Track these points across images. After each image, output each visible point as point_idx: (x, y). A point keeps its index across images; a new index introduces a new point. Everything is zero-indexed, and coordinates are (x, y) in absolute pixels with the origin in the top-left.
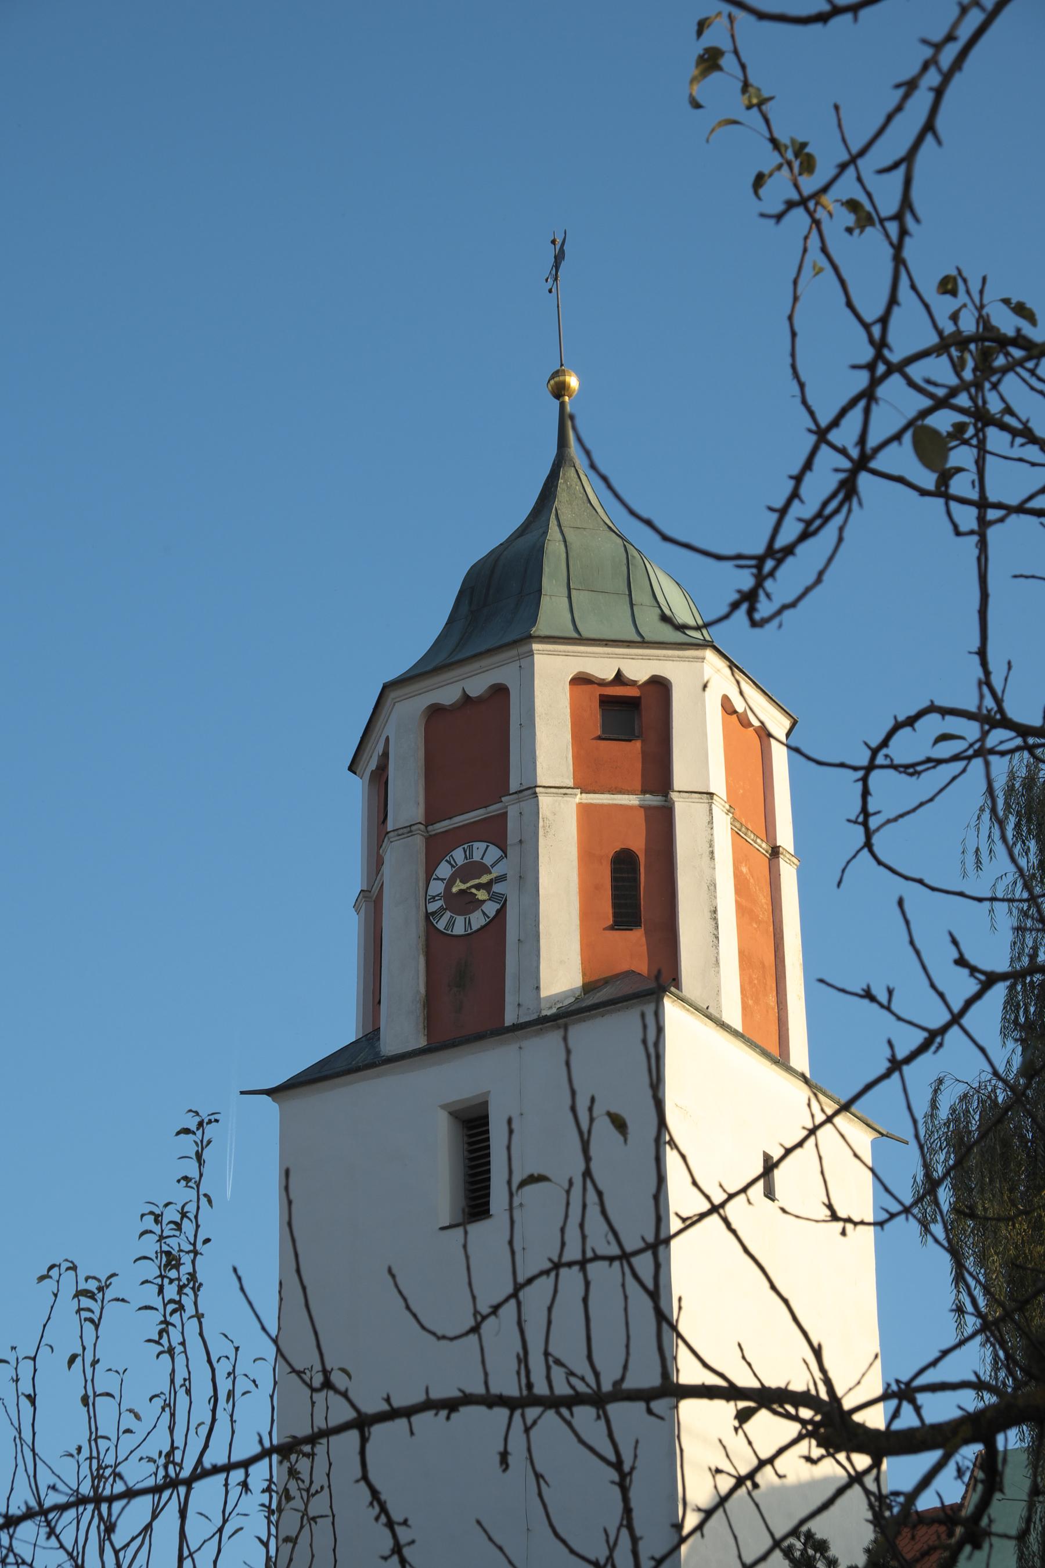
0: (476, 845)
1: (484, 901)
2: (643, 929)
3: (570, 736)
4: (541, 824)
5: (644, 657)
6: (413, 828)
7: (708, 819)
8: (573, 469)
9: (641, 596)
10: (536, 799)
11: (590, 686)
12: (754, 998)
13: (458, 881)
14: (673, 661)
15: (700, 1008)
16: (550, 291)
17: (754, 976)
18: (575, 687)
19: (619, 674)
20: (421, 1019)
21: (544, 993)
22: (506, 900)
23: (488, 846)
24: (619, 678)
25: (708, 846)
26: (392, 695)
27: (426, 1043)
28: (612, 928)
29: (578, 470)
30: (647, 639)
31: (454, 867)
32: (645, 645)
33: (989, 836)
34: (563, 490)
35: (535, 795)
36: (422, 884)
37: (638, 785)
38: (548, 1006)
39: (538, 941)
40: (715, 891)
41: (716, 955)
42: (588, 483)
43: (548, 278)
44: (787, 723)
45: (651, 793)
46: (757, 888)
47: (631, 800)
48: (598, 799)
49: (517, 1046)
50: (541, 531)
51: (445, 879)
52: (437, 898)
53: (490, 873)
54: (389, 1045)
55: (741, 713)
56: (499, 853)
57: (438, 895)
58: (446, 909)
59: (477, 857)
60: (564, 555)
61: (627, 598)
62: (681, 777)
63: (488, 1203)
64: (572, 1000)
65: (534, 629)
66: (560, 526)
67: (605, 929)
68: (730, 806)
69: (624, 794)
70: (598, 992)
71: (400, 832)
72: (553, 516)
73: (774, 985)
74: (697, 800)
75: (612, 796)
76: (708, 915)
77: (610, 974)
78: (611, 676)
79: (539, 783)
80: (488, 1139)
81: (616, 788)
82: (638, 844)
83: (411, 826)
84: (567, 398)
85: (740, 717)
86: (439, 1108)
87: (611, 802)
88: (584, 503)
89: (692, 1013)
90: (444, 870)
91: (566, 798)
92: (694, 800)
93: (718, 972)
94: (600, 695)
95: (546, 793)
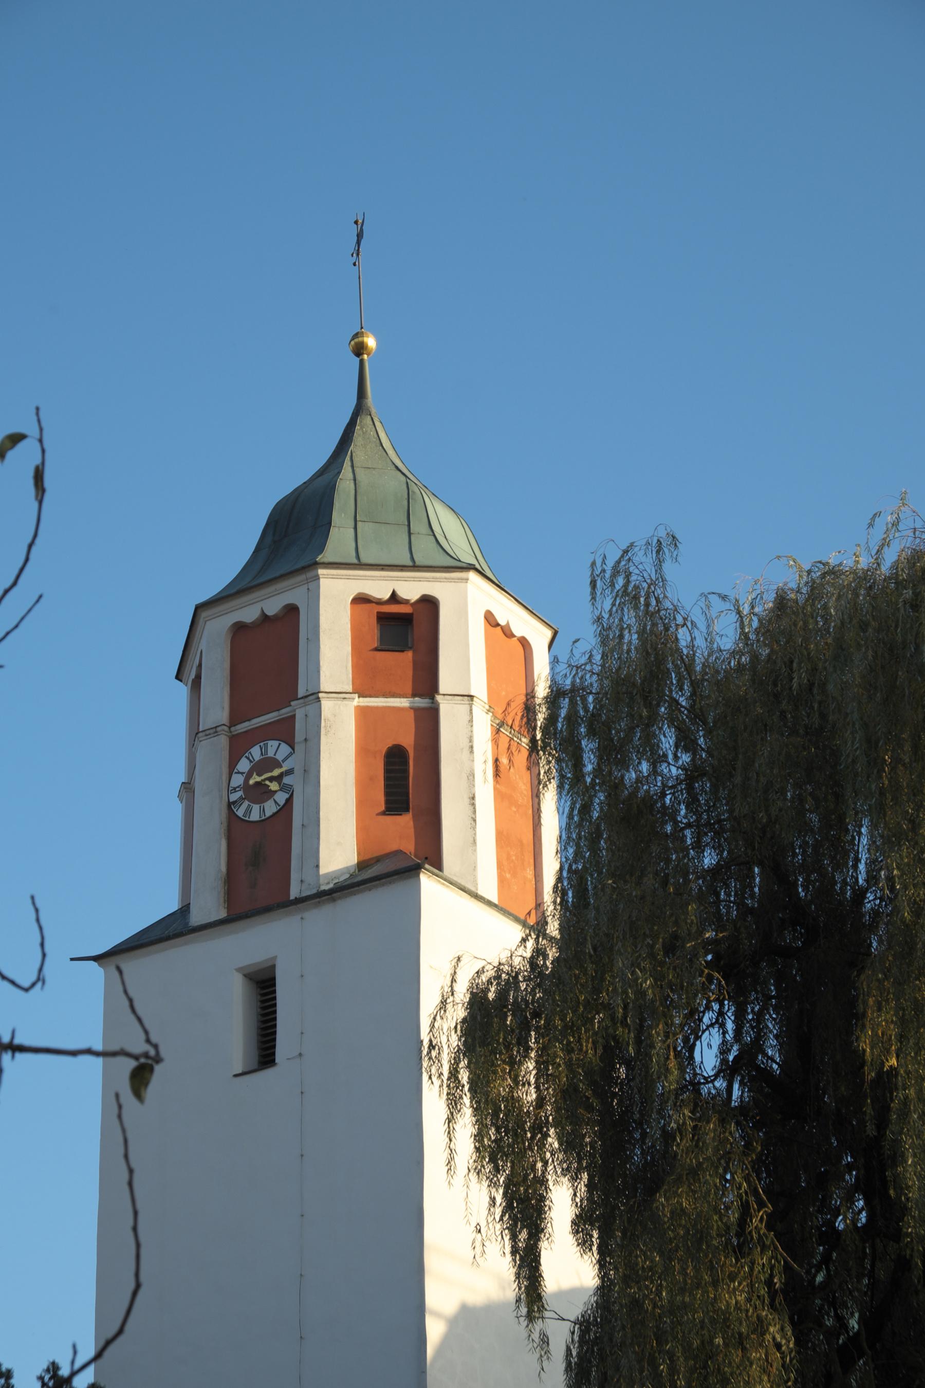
0: (270, 743)
1: (275, 792)
2: (411, 813)
3: (349, 648)
4: (323, 724)
5: (415, 579)
6: (219, 729)
7: (468, 718)
8: (369, 417)
9: (418, 526)
10: (319, 703)
11: (368, 605)
12: (511, 872)
13: (255, 774)
14: (441, 582)
15: (454, 882)
16: (355, 264)
17: (512, 853)
18: (356, 606)
19: (394, 594)
20: (222, 894)
21: (323, 870)
22: (293, 791)
23: (280, 744)
24: (394, 598)
25: (468, 741)
26: (204, 614)
27: (226, 915)
28: (384, 813)
29: (374, 417)
30: (418, 563)
31: (252, 762)
32: (416, 569)
33: (509, 749)
34: (359, 435)
35: (318, 700)
36: (225, 777)
37: (409, 688)
38: (326, 882)
39: (319, 825)
40: (474, 781)
41: (474, 836)
42: (383, 429)
43: (353, 253)
44: (549, 634)
45: (420, 696)
46: (517, 777)
47: (403, 702)
48: (373, 702)
49: (299, 917)
50: (336, 471)
51: (244, 773)
52: (237, 789)
53: (281, 767)
54: (196, 918)
55: (505, 626)
56: (289, 750)
57: (238, 787)
58: (244, 799)
59: (271, 754)
60: (353, 492)
61: (406, 528)
62: (447, 681)
63: (274, 1054)
64: (347, 876)
65: (320, 557)
66: (352, 466)
67: (378, 814)
68: (490, 706)
69: (396, 697)
70: (370, 869)
71: (208, 732)
72: (348, 458)
73: (532, 861)
74: (459, 702)
75: (386, 699)
76: (467, 801)
77: (382, 854)
78: (386, 596)
79: (322, 689)
80: (275, 998)
81: (390, 692)
82: (407, 740)
83: (216, 727)
84: (365, 357)
85: (504, 629)
86: (235, 971)
87: (384, 704)
88: (377, 446)
89: (447, 886)
90: (244, 765)
91: (345, 702)
92: (456, 702)
93: (475, 850)
94: (378, 613)
95: (328, 698)
